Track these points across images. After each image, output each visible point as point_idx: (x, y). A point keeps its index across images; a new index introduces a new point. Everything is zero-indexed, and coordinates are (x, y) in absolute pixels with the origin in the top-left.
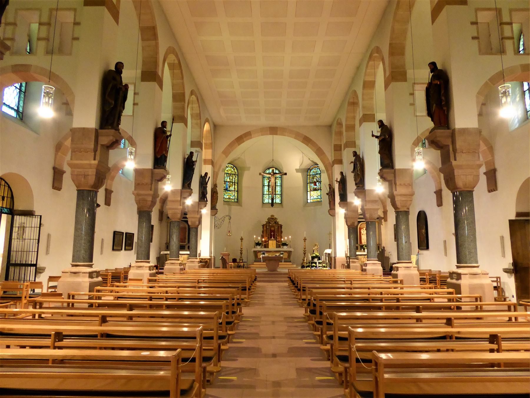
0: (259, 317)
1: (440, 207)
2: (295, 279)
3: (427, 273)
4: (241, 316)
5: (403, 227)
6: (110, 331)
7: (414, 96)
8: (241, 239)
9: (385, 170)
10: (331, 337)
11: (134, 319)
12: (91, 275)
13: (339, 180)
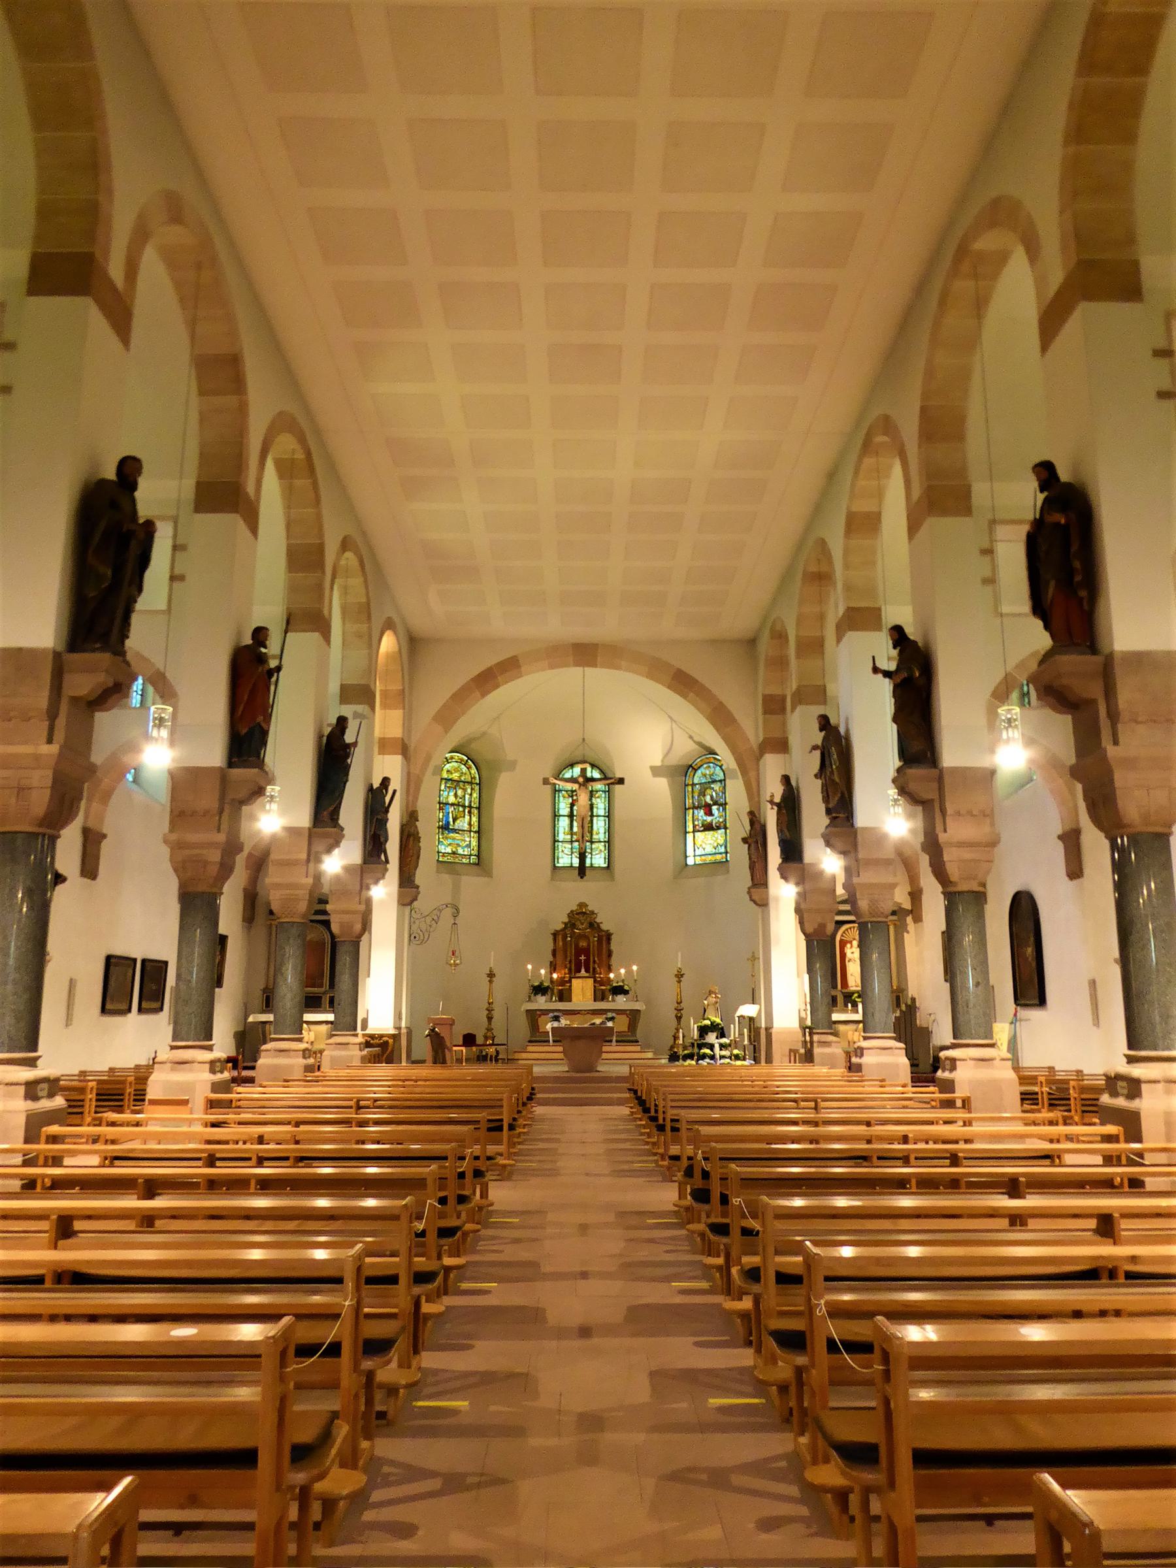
0: (540, 1212)
1: (1075, 882)
2: (649, 1092)
3: (1043, 1079)
4: (485, 1210)
5: (968, 939)
6: (89, 1262)
7: (993, 560)
8: (676, 976)
9: (913, 772)
10: (753, 1275)
11: (159, 1224)
12: (32, 1090)
13: (777, 799)
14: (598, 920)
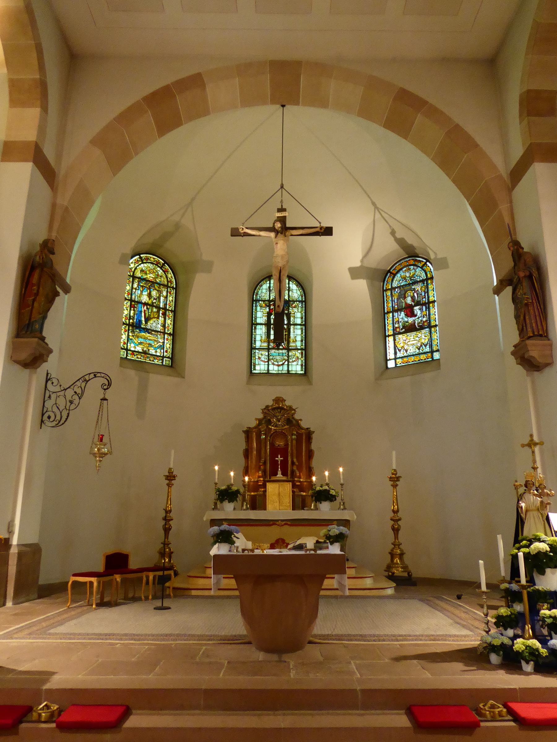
14: (297, 417)
